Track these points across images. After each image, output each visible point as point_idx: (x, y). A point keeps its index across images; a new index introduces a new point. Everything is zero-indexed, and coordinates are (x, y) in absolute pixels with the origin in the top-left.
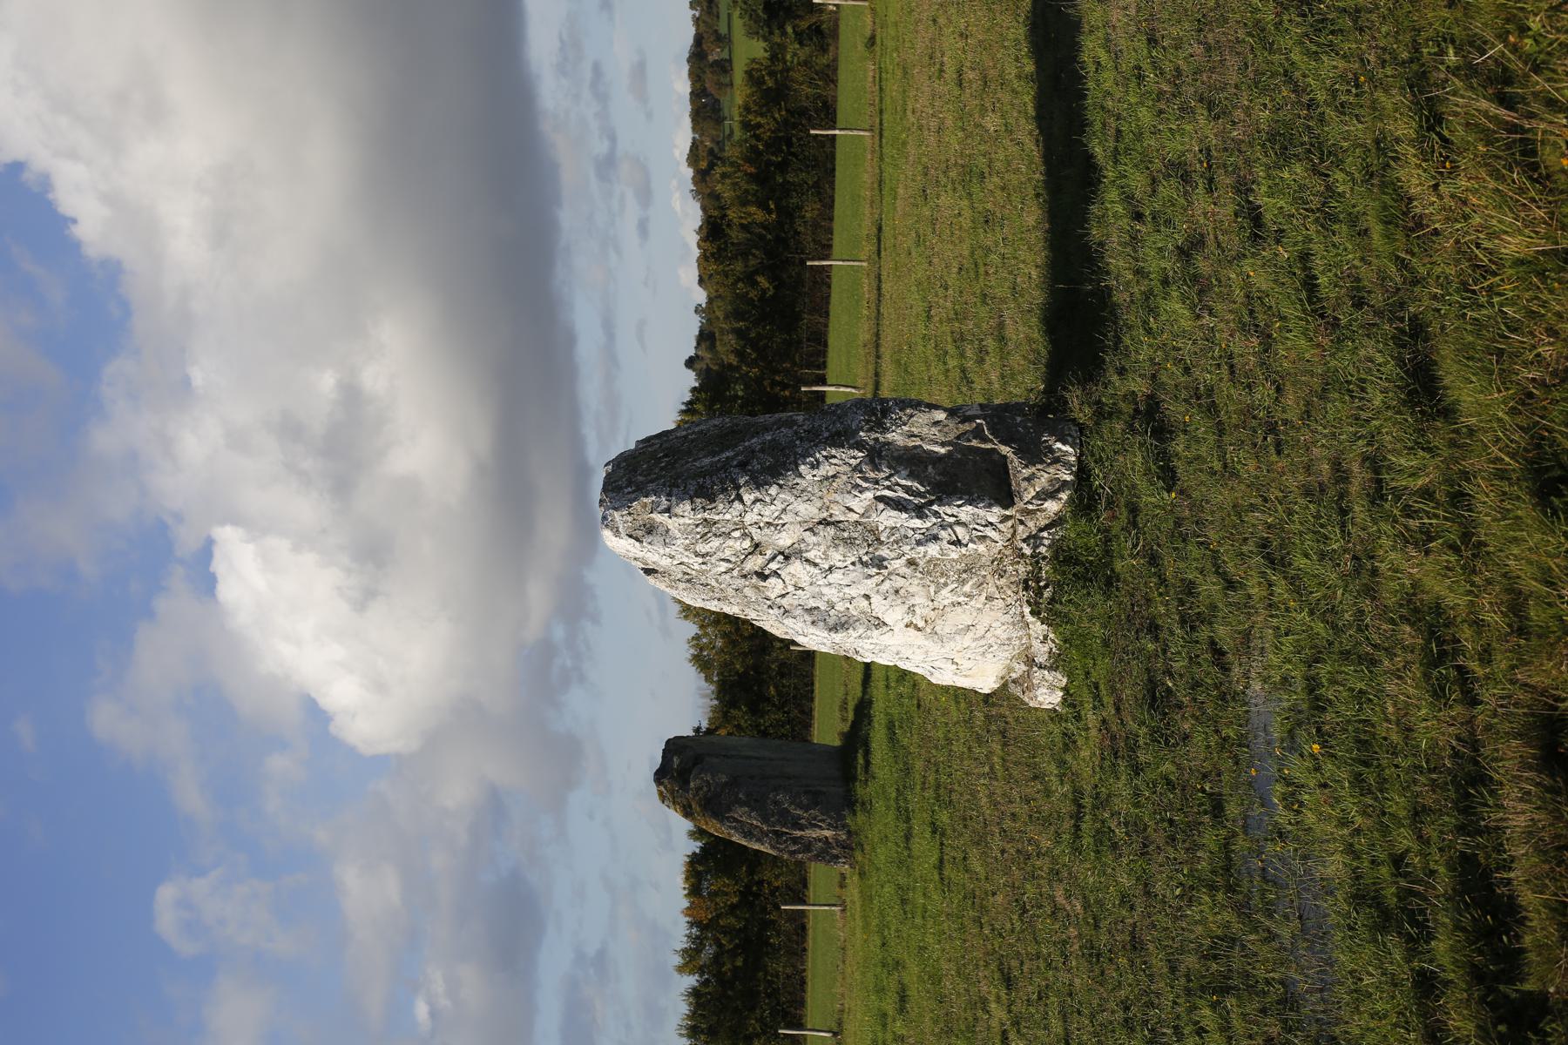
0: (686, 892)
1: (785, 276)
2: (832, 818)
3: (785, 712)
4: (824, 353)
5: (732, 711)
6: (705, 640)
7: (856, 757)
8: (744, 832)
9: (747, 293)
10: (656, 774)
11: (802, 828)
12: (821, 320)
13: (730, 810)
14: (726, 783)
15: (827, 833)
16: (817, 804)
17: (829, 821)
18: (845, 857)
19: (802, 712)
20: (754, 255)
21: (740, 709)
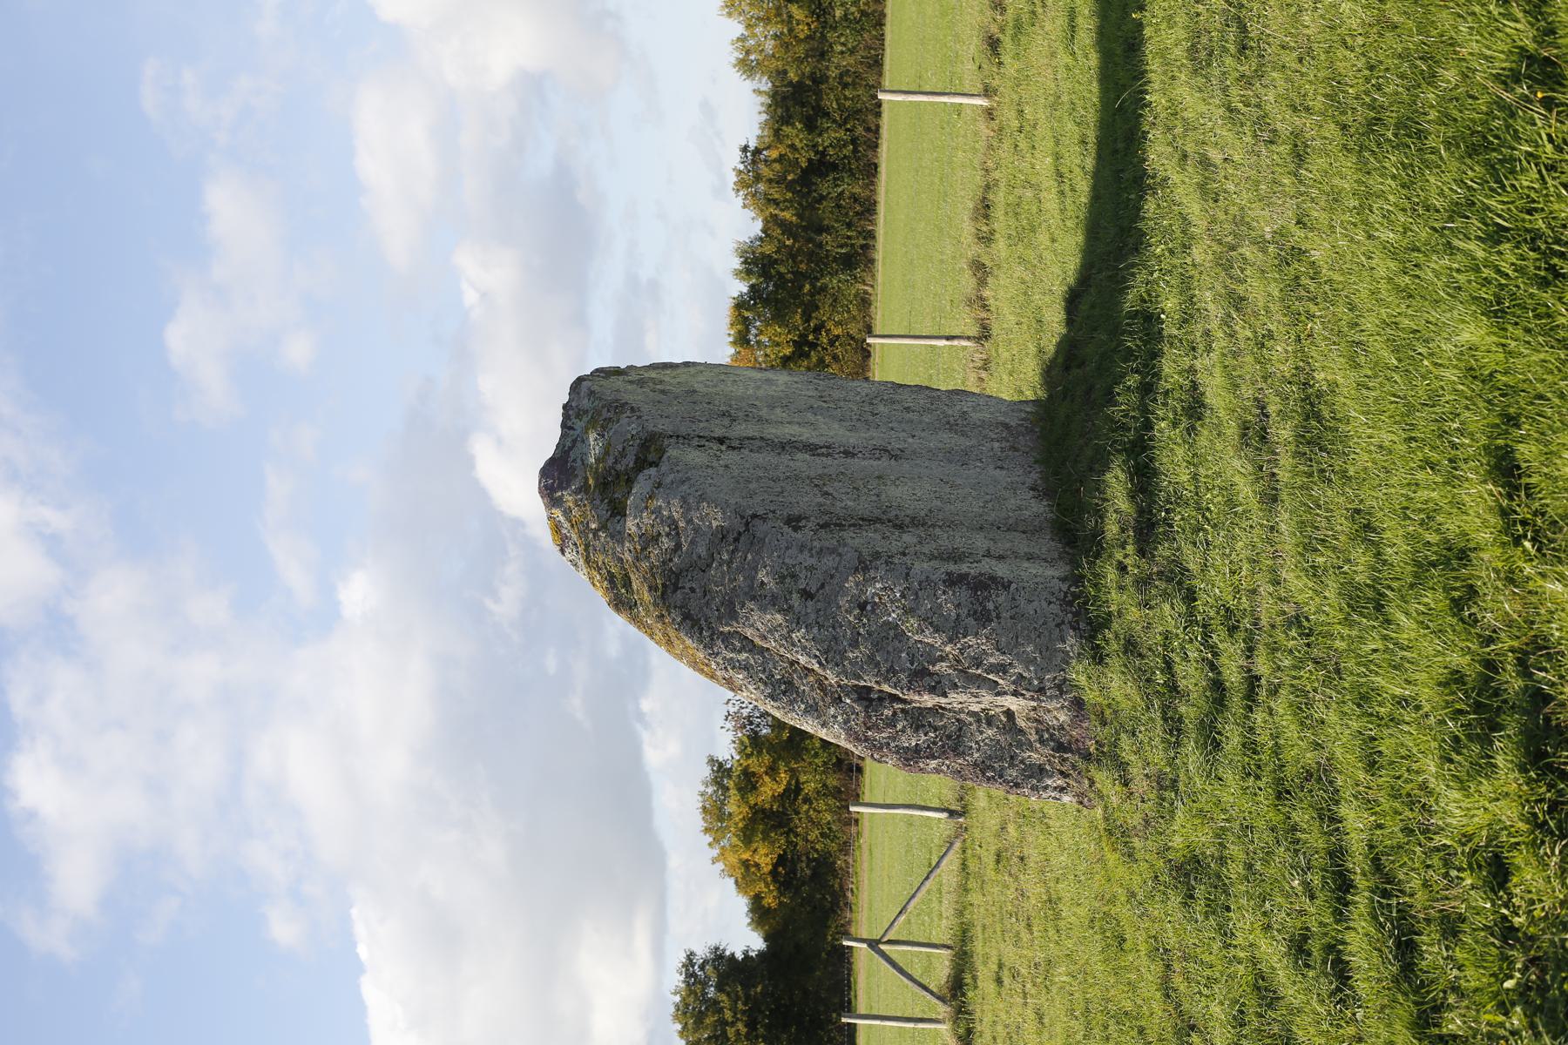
0: (731, 339)
2: (1028, 662)
3: (847, 130)
5: (784, 128)
6: (752, 42)
7: (1100, 487)
8: (769, 681)
10: (545, 472)
11: (938, 687)
13: (733, 615)
14: (722, 535)
15: (1011, 703)
16: (983, 617)
17: (1019, 669)
18: (1064, 774)
19: (868, 129)
21: (793, 125)
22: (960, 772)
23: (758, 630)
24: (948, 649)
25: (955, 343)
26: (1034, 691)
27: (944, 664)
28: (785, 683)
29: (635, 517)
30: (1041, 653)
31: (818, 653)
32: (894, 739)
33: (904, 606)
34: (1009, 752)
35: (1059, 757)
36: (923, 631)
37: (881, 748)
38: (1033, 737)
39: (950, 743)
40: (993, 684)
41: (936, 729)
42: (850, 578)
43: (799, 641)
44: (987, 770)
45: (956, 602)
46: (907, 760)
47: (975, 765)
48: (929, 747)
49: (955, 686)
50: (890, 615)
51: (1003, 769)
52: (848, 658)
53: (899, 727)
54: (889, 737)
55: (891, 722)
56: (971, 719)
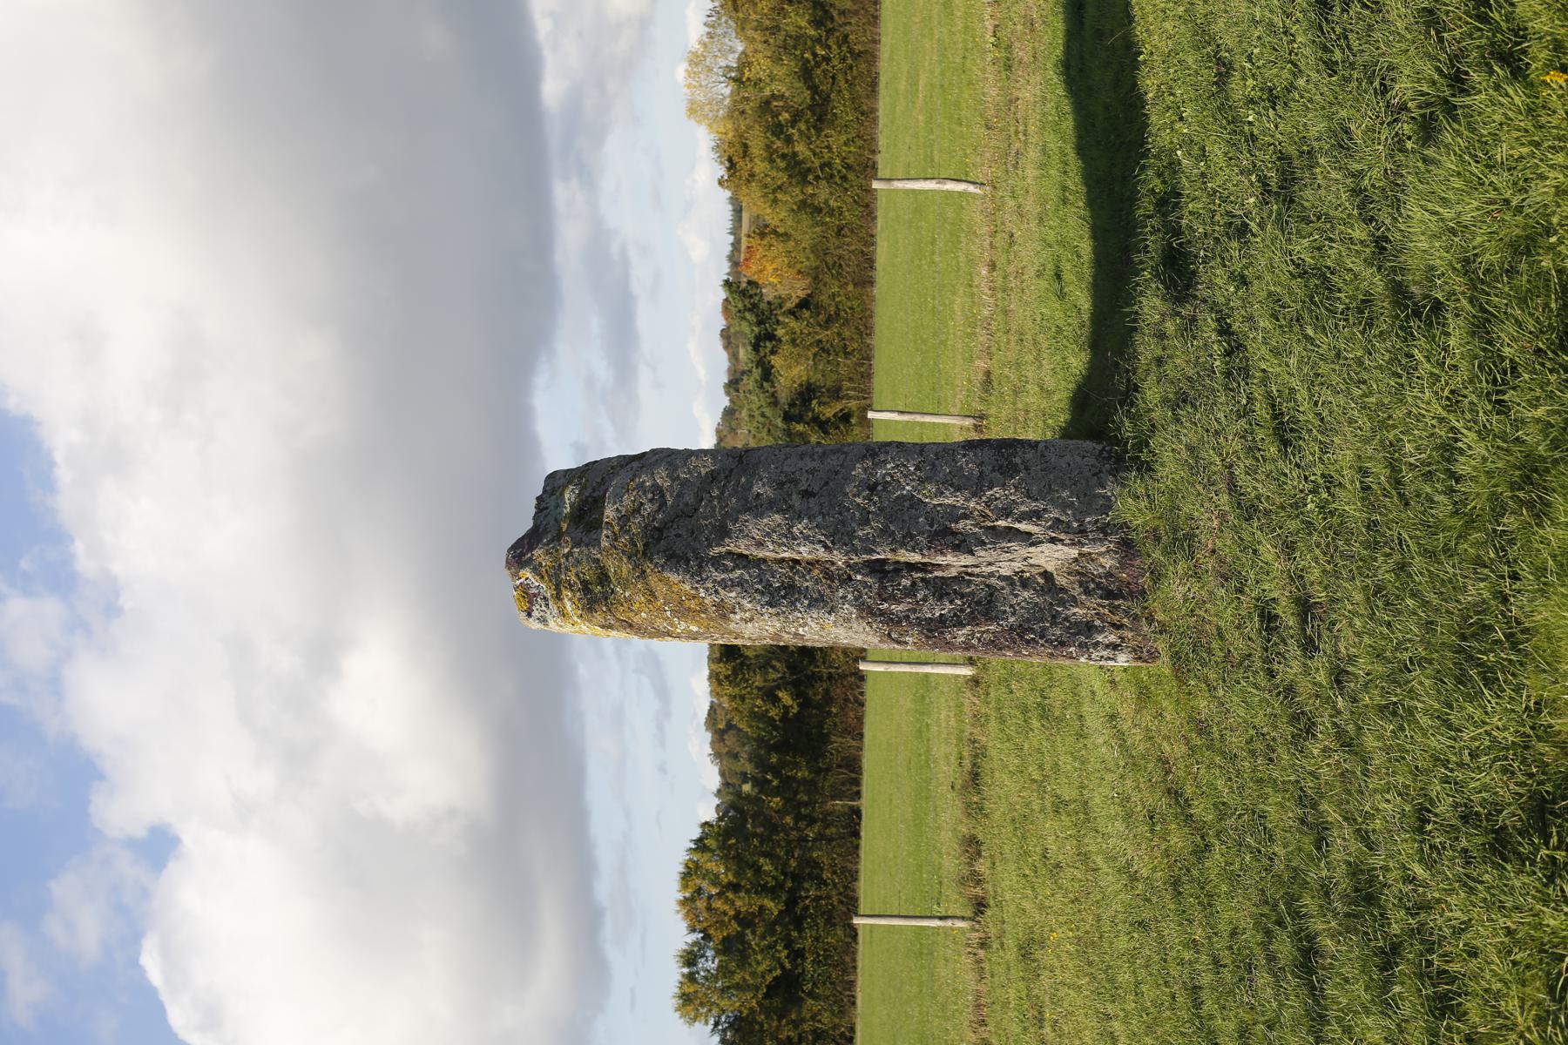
1: (811, 693)
2: (1064, 506)
4: (857, 782)
9: (767, 711)
11: (963, 545)
12: (854, 743)
13: (723, 533)
15: (1052, 557)
17: (1055, 514)
20: (774, 667)
22: (993, 641)
23: (753, 538)
24: (972, 505)
25: (949, 923)
26: (1074, 533)
27: (968, 522)
28: (785, 588)
29: (615, 503)
30: (1078, 498)
31: (823, 538)
32: (914, 611)
33: (920, 477)
34: (1050, 611)
35: (1109, 605)
36: (943, 493)
37: (899, 622)
38: (1076, 591)
39: (980, 608)
40: (1025, 536)
41: (962, 596)
42: (858, 465)
43: (801, 533)
44: (1022, 635)
45: (978, 462)
46: (931, 631)
47: (1011, 629)
48: (955, 615)
49: (983, 543)
50: (904, 489)
51: (1044, 629)
52: (856, 537)
53: (919, 596)
54: (908, 610)
55: (911, 592)
56: (1003, 584)
